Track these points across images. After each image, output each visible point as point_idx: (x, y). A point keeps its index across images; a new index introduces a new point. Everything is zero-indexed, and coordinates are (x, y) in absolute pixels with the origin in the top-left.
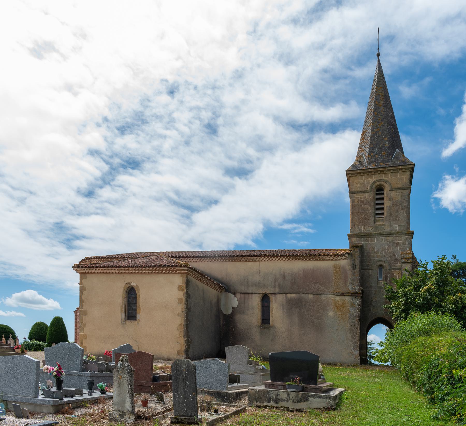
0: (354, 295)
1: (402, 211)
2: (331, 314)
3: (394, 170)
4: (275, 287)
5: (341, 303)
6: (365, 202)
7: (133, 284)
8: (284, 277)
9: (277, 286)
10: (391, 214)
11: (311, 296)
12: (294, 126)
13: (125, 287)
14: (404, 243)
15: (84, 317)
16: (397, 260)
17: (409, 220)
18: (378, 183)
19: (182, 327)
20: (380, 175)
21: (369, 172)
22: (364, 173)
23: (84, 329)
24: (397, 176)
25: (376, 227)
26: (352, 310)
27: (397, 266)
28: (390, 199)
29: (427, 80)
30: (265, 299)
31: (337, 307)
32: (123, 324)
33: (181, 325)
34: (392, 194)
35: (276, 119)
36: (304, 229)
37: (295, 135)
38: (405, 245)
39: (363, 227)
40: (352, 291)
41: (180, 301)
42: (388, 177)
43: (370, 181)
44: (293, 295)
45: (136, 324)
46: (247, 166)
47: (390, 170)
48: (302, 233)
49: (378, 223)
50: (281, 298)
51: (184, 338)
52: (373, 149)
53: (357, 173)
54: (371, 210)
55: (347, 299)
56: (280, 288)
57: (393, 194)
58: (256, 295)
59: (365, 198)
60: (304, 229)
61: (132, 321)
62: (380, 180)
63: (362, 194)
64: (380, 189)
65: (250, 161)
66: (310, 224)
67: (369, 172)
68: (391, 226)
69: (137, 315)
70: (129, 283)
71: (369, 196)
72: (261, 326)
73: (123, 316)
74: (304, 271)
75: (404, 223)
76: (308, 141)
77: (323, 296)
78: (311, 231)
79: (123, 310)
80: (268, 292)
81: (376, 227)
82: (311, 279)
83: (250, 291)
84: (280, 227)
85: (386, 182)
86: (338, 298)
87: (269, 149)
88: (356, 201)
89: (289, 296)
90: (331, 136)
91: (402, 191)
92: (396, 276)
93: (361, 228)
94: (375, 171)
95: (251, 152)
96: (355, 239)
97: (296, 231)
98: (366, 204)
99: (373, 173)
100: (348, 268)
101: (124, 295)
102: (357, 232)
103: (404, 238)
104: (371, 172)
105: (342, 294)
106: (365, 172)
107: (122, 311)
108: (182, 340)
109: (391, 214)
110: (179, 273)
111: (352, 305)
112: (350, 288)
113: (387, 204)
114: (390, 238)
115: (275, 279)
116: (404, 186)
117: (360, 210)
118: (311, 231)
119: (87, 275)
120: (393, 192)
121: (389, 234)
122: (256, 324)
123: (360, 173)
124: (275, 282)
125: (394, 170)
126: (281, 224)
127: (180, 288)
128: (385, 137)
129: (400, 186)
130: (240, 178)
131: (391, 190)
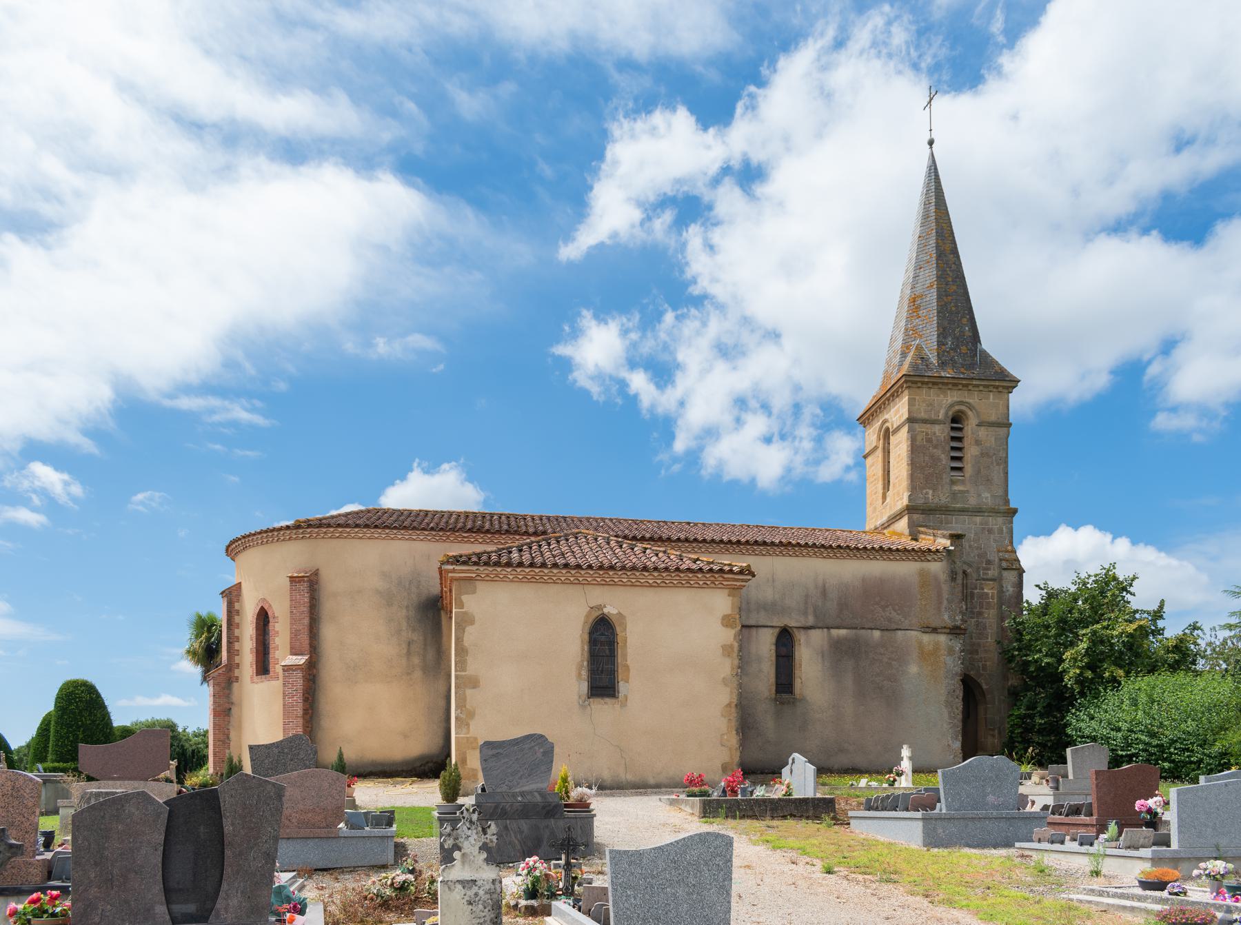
0: (955, 631)
2: (913, 669)
3: (985, 386)
4: (805, 613)
5: (931, 647)
7: (610, 610)
8: (824, 593)
9: (810, 610)
10: (979, 472)
11: (877, 634)
12: (193, 126)
13: (587, 616)
14: (1001, 531)
15: (469, 692)
16: (989, 562)
18: (957, 408)
19: (733, 710)
21: (943, 384)
22: (934, 383)
23: (468, 725)
24: (988, 398)
25: (954, 495)
26: (949, 660)
27: (991, 573)
28: (978, 443)
29: (508, 88)
30: (785, 639)
31: (926, 656)
32: (583, 707)
33: (729, 705)
35: (126, 87)
36: (240, 413)
37: (185, 148)
39: (931, 492)
40: (950, 623)
41: (726, 650)
42: (974, 399)
43: (945, 401)
44: (843, 632)
45: (617, 706)
46: (48, 210)
47: (978, 386)
48: (234, 424)
49: (956, 488)
50: (818, 637)
51: (738, 733)
53: (923, 383)
54: (945, 460)
55: (942, 639)
56: (816, 616)
57: (982, 432)
58: (766, 630)
60: (240, 413)
61: (607, 700)
64: (957, 420)
65: (47, 194)
66: (258, 403)
67: (943, 384)
68: (979, 495)
69: (621, 684)
70: (600, 607)
71: (941, 432)
72: (776, 700)
73: (585, 687)
74: (864, 580)
75: (1000, 492)
76: (226, 173)
77: (899, 632)
78: (258, 420)
79: (584, 673)
80: (792, 624)
81: (954, 495)
82: (877, 599)
83: (752, 622)
84: (167, 403)
85: (971, 407)
86: (926, 638)
87: (117, 172)
88: (919, 438)
89: (834, 632)
90: (287, 170)
92: (987, 594)
94: (954, 384)
95: (54, 168)
97: (216, 418)
98: (935, 447)
100: (943, 577)
101: (586, 637)
103: (1000, 520)
104: (947, 384)
105: (935, 630)
106: (938, 383)
107: (580, 675)
108: (734, 740)
109: (979, 472)
110: (726, 587)
111: (951, 651)
112: (946, 617)
113: (971, 452)
114: (978, 519)
115: (807, 596)
117: (927, 458)
118: (258, 420)
119: (478, 583)
121: (978, 511)
122: (766, 694)
123: (927, 383)
124: (806, 603)
125: (985, 386)
126: (171, 396)
127: (727, 621)
129: (993, 418)
130: (24, 240)
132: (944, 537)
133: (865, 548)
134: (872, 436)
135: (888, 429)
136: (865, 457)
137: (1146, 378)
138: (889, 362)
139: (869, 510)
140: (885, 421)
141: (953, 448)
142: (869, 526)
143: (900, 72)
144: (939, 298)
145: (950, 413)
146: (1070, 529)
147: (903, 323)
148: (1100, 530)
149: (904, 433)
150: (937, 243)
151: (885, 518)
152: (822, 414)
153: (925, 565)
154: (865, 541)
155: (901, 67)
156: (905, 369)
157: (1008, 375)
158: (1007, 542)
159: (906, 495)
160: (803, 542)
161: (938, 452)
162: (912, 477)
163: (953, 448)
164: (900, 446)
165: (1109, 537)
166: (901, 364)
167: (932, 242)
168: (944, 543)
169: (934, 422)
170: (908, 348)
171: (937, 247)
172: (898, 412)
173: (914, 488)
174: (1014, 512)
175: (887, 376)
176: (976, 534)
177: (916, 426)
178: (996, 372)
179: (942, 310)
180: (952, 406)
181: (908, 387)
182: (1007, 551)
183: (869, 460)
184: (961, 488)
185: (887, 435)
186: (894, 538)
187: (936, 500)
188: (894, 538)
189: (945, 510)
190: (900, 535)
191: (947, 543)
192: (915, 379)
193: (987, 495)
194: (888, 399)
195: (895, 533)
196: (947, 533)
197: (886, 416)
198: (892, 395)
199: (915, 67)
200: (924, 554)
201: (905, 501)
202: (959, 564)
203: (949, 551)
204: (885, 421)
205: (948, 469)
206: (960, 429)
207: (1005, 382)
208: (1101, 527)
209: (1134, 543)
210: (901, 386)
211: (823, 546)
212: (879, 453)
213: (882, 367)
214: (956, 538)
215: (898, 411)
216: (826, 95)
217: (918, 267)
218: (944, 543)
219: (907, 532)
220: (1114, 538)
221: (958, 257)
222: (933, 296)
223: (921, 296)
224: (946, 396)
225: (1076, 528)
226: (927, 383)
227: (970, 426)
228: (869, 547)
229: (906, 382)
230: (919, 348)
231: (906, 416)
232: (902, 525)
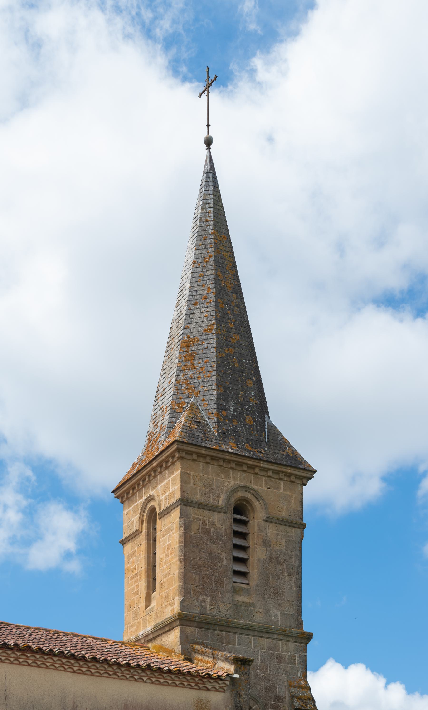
1: (288, 578)
6: (214, 535)
10: (266, 581)
14: (292, 660)
17: (300, 603)
18: (241, 494)
20: (245, 474)
21: (224, 460)
22: (213, 458)
24: (278, 488)
28: (266, 543)
34: (269, 531)
38: (294, 664)
39: (208, 600)
42: (261, 486)
43: (227, 483)
47: (266, 470)
49: (240, 598)
52: (226, 400)
54: (225, 559)
57: (271, 531)
59: (214, 524)
62: (245, 489)
63: (206, 512)
64: (240, 510)
67: (224, 460)
68: (267, 611)
71: (222, 522)
75: (292, 611)
81: (237, 607)
85: (258, 496)
88: (194, 527)
91: (288, 528)
93: (204, 601)
94: (237, 463)
96: (192, 629)
98: (214, 541)
99: (233, 465)
102: (198, 611)
103: (292, 646)
104: (229, 461)
106: (216, 458)
113: (257, 554)
114: (266, 642)
116: (292, 518)
117: (203, 555)
120: (271, 525)
121: (265, 631)
123: (205, 456)
128: (247, 378)
129: (284, 515)
131: (268, 520)
132: (227, 660)
133: (128, 665)
134: (131, 517)
135: (153, 510)
136: (123, 543)
137: (420, 493)
138: (154, 422)
139: (128, 614)
140: (150, 499)
141: (236, 547)
142: (129, 636)
143: (128, 37)
144: (219, 347)
145: (233, 500)
146: (339, 666)
147: (173, 373)
148: (373, 671)
149: (175, 517)
150: (216, 275)
151: (149, 628)
152: (34, 479)
153: (204, 694)
154: (126, 655)
155: (130, 30)
156: (177, 432)
157: (302, 461)
158: (299, 674)
159: (177, 600)
160: (46, 648)
161: (217, 548)
162: (185, 577)
163: (236, 547)
164: (170, 534)
165: (382, 681)
166: (171, 425)
167: (211, 272)
168: (225, 668)
169: (213, 509)
170: (180, 406)
171: (217, 280)
172: (167, 489)
173: (187, 592)
174: (309, 637)
175: (152, 439)
176: (263, 661)
177: (191, 510)
178: (287, 456)
179: (223, 364)
180: (234, 490)
181: (181, 458)
182: (300, 687)
183: (129, 548)
184: (246, 599)
185: (152, 517)
186: (162, 655)
187: (215, 612)
188: (162, 655)
189: (227, 626)
190: (170, 652)
191: (231, 668)
192: (187, 448)
193: (275, 611)
194: (154, 470)
195: (162, 649)
196: (231, 655)
197: (152, 493)
198: (160, 465)
199: (148, 33)
200: (202, 680)
201: (176, 608)
202: (244, 697)
203: (233, 680)
204: (150, 499)
205: (230, 573)
206: (245, 523)
207: (303, 472)
208: (374, 667)
209: (410, 691)
210: (172, 455)
211: (73, 656)
212: (142, 540)
213: (144, 427)
214: (241, 663)
215: (167, 487)
216: (35, 45)
217: (193, 302)
218: (225, 668)
219: (178, 648)
220: (388, 683)
221: (242, 298)
222: (211, 342)
223: (196, 341)
224: (227, 476)
225: (346, 666)
226: (205, 456)
227: (257, 519)
228: (133, 663)
229: (178, 450)
230: (194, 409)
231: (177, 496)
232: (172, 639)
